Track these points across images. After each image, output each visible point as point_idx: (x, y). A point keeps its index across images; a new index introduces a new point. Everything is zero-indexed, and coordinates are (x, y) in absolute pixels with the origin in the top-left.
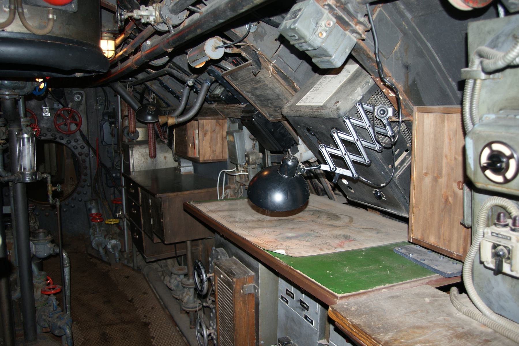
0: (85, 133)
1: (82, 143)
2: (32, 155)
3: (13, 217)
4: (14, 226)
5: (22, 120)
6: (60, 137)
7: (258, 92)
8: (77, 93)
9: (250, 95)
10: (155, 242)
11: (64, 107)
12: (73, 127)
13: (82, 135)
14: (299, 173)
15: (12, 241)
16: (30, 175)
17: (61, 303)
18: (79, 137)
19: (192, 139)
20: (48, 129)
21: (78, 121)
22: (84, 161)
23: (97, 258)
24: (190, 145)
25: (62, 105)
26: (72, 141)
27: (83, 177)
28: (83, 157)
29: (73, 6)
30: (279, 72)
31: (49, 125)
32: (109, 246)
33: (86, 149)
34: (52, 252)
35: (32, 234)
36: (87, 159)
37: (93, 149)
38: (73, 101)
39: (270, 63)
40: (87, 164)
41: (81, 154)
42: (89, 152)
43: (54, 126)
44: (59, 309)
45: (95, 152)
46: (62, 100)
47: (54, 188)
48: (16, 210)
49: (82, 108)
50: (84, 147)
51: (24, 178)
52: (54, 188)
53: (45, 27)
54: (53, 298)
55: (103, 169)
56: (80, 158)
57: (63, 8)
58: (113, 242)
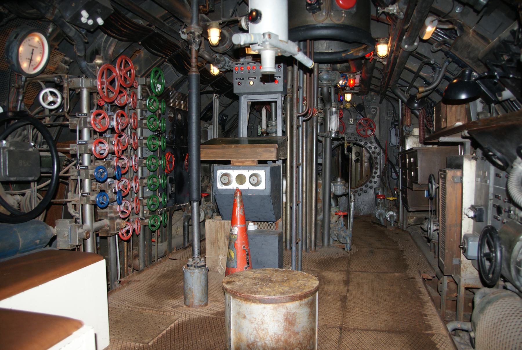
0: (378, 137)
1: (375, 145)
2: (337, 121)
3: (323, 165)
4: (323, 173)
5: (333, 104)
6: (360, 140)
7: (472, 55)
8: (373, 108)
9: (467, 60)
10: (413, 190)
11: (364, 117)
12: (369, 132)
13: (376, 138)
14: (474, 79)
15: (321, 182)
16: (335, 132)
17: (346, 225)
18: (373, 140)
19: (444, 115)
20: (352, 134)
21: (373, 127)
22: (376, 158)
23: (378, 224)
24: (443, 120)
25: (363, 116)
26: (368, 143)
27: (374, 170)
28: (376, 155)
29: (354, 9)
30: (478, 34)
31: (352, 131)
32: (387, 216)
33: (377, 150)
34: (344, 191)
35: (333, 179)
36: (378, 157)
37: (383, 149)
38: (370, 113)
39: (471, 28)
40: (378, 161)
41: (374, 153)
42: (380, 151)
43: (356, 132)
44: (345, 227)
45: (384, 152)
46: (362, 113)
47: (348, 145)
48: (325, 162)
49: (376, 119)
50: (377, 148)
51: (331, 135)
52: (348, 145)
53: (340, 20)
54: (342, 219)
55: (389, 164)
56: (373, 156)
57: (349, 10)
58: (391, 213)
